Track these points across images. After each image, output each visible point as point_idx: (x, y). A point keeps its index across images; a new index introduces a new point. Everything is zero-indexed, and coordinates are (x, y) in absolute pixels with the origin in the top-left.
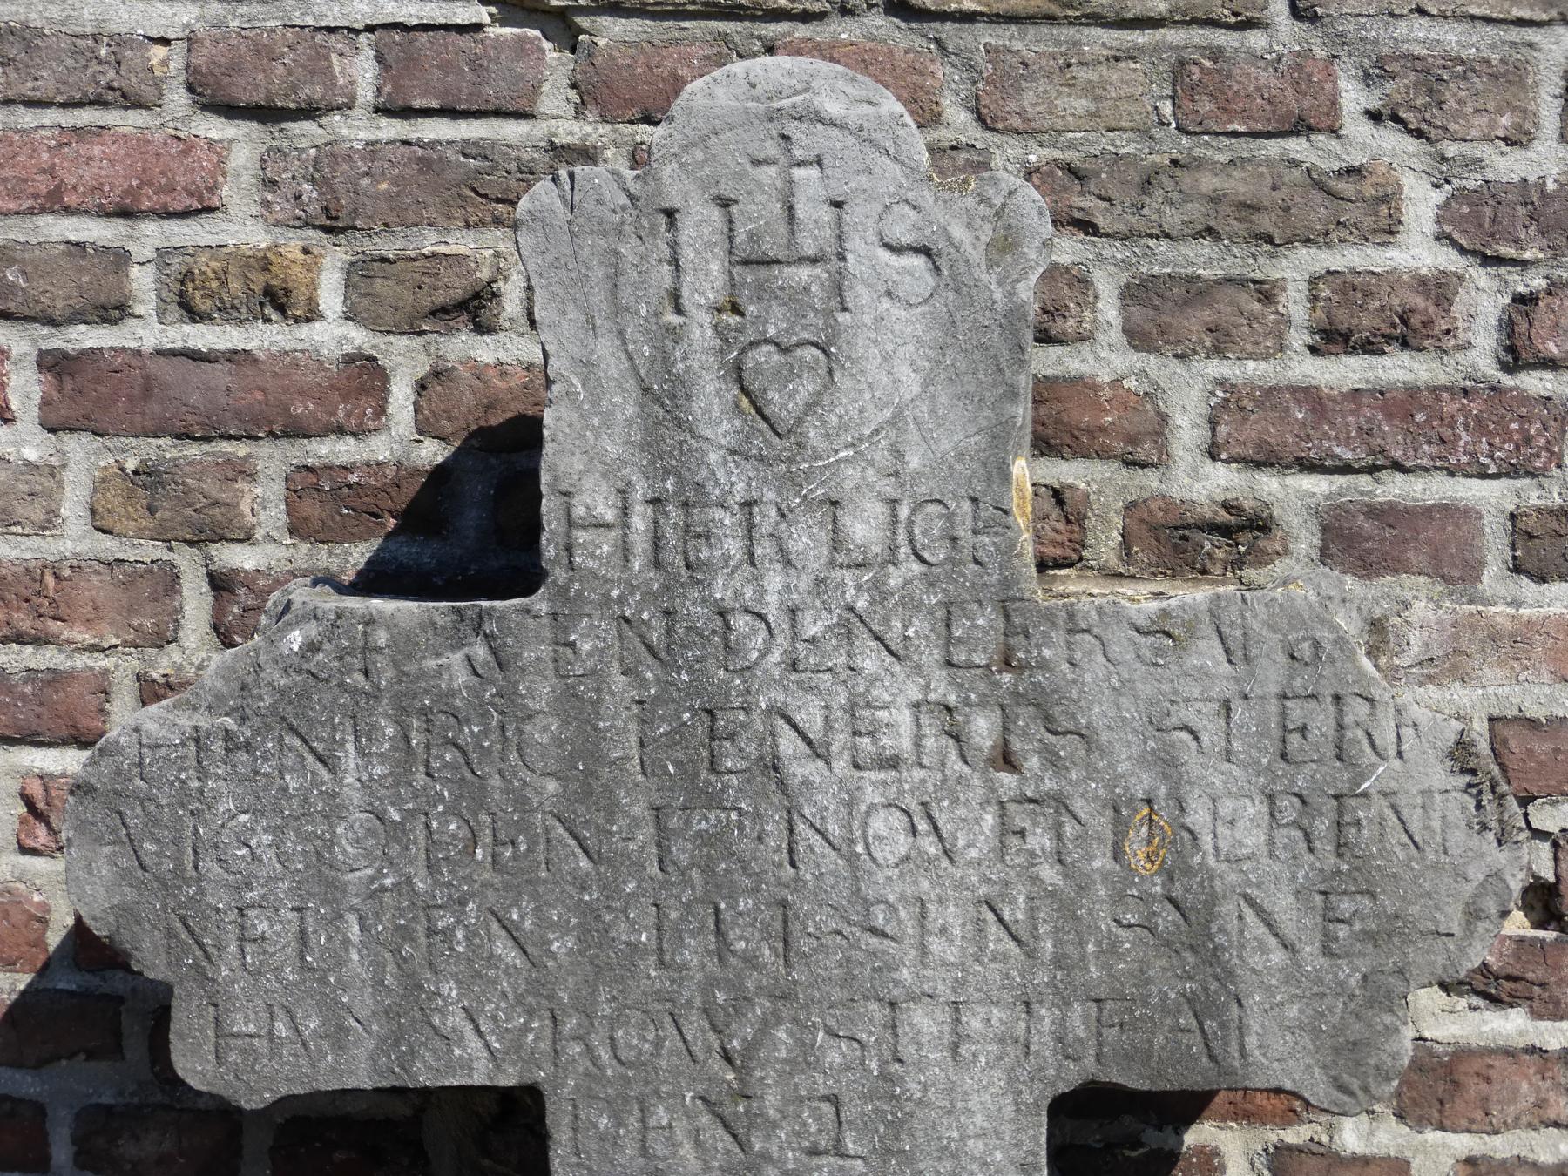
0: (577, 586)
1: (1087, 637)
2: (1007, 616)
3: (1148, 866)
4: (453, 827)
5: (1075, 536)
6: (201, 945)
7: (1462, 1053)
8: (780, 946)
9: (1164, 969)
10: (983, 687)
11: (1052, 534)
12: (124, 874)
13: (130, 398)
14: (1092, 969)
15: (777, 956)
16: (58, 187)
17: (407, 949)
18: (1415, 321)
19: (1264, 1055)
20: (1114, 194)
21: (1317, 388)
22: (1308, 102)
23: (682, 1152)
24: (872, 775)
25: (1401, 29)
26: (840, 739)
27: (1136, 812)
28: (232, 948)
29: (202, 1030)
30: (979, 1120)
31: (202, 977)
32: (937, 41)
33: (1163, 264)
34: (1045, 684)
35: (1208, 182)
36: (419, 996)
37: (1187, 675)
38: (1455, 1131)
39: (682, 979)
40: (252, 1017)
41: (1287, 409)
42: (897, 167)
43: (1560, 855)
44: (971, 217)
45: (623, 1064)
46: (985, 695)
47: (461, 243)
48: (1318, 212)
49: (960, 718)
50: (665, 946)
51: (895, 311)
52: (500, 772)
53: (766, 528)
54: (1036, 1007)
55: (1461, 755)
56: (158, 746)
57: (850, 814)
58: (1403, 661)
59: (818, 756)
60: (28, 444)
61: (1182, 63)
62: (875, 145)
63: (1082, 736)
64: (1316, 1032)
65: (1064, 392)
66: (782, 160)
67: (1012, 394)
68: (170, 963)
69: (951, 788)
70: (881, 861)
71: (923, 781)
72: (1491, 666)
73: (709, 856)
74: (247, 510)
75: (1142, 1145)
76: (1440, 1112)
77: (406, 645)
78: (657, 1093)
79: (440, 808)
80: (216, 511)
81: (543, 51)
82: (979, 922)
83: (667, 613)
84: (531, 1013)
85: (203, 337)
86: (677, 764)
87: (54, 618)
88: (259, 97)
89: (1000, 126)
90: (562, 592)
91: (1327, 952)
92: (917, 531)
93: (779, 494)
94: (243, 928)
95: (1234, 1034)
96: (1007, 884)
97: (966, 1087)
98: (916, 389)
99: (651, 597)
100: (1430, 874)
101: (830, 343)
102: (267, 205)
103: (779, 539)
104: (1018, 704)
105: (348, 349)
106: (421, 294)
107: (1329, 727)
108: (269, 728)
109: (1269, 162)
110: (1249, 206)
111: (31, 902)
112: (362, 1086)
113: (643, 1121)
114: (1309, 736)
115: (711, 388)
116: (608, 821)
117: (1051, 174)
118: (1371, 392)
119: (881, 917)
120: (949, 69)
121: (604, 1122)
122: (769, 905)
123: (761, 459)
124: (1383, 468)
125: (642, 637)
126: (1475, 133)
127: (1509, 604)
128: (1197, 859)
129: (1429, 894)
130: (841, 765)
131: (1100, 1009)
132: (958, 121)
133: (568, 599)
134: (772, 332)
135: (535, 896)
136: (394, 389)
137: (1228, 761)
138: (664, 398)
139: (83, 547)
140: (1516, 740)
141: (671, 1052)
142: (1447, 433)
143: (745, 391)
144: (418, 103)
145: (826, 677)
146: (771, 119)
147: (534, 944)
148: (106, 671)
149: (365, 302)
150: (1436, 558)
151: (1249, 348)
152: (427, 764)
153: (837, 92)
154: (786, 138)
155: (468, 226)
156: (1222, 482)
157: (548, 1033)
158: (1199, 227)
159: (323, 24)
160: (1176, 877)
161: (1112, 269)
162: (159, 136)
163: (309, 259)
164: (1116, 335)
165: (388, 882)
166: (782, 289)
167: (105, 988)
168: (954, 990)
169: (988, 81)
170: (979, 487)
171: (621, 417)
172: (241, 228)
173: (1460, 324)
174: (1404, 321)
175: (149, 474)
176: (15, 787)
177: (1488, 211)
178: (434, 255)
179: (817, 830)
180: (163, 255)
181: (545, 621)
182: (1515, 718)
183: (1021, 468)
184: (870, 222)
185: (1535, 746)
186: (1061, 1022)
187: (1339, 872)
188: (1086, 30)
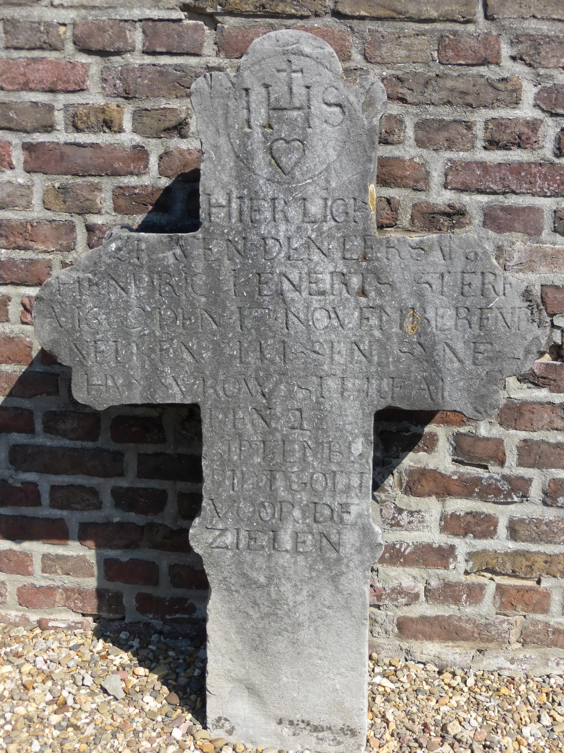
0: (212, 228)
1: (393, 249)
2: (365, 242)
5: (394, 216)
6: (82, 354)
7: (524, 403)
8: (282, 357)
10: (356, 267)
11: (386, 215)
12: (54, 329)
13: (56, 161)
16: (27, 81)
17: (153, 356)
18: (524, 137)
20: (414, 88)
21: (486, 162)
22: (488, 52)
25: (526, 24)
26: (305, 285)
27: (408, 312)
28: (92, 355)
29: (83, 383)
30: (350, 418)
31: (82, 364)
32: (351, 27)
33: (431, 115)
34: (378, 266)
35: (449, 83)
37: (428, 264)
41: (474, 170)
42: (330, 73)
44: (357, 93)
47: (175, 104)
48: (490, 95)
51: (328, 128)
52: (185, 294)
53: (280, 208)
55: (527, 295)
56: (65, 284)
58: (511, 264)
60: (21, 178)
61: (442, 37)
62: (322, 64)
64: (469, 391)
65: (392, 163)
66: (288, 70)
67: (370, 160)
68: (71, 360)
69: (343, 302)
71: (334, 300)
72: (543, 266)
73: (258, 325)
74: (99, 202)
77: (152, 250)
78: (239, 406)
80: (87, 202)
81: (204, 30)
82: (352, 350)
83: (244, 238)
84: (196, 378)
85: (82, 138)
86: (246, 292)
87: (31, 241)
88: (100, 47)
89: (373, 61)
90: (207, 230)
91: (474, 364)
92: (334, 210)
93: (285, 196)
94: (96, 348)
95: (440, 391)
96: (362, 336)
98: (335, 158)
99: (238, 233)
100: (513, 337)
101: (304, 140)
102: (103, 88)
103: (284, 212)
105: (134, 143)
106: (160, 123)
107: (479, 284)
108: (104, 278)
109: (473, 76)
110: (464, 93)
111: (26, 341)
113: (234, 416)
115: (261, 156)
117: (391, 80)
118: (505, 164)
120: (355, 38)
121: (221, 416)
122: (279, 342)
123: (278, 182)
124: (508, 193)
125: (235, 247)
126: (551, 65)
127: (551, 244)
128: (429, 329)
130: (305, 294)
132: (357, 59)
133: (209, 233)
134: (283, 135)
135: (197, 338)
136: (151, 159)
138: (244, 159)
139: (41, 215)
140: (550, 294)
141: (244, 392)
142: (533, 180)
143: (273, 157)
144: (158, 50)
145: (300, 262)
146: (284, 54)
149: (140, 126)
150: (525, 226)
151: (461, 147)
152: (160, 291)
153: (309, 44)
154: (290, 61)
155: (177, 97)
156: (448, 197)
157: (202, 385)
158: (445, 101)
159: (123, 18)
161: (412, 116)
162: (63, 62)
163: (119, 109)
164: (412, 142)
165: (146, 332)
166: (287, 119)
168: (342, 373)
169: (369, 43)
170: (356, 194)
171: (228, 167)
172: (94, 97)
173: (540, 139)
174: (520, 138)
175: (64, 189)
176: (19, 301)
177: (554, 96)
178: (165, 108)
180: (66, 107)
181: (201, 241)
182: (551, 285)
183: (372, 187)
184: (320, 94)
185: (557, 295)
186: (379, 386)
188: (407, 23)
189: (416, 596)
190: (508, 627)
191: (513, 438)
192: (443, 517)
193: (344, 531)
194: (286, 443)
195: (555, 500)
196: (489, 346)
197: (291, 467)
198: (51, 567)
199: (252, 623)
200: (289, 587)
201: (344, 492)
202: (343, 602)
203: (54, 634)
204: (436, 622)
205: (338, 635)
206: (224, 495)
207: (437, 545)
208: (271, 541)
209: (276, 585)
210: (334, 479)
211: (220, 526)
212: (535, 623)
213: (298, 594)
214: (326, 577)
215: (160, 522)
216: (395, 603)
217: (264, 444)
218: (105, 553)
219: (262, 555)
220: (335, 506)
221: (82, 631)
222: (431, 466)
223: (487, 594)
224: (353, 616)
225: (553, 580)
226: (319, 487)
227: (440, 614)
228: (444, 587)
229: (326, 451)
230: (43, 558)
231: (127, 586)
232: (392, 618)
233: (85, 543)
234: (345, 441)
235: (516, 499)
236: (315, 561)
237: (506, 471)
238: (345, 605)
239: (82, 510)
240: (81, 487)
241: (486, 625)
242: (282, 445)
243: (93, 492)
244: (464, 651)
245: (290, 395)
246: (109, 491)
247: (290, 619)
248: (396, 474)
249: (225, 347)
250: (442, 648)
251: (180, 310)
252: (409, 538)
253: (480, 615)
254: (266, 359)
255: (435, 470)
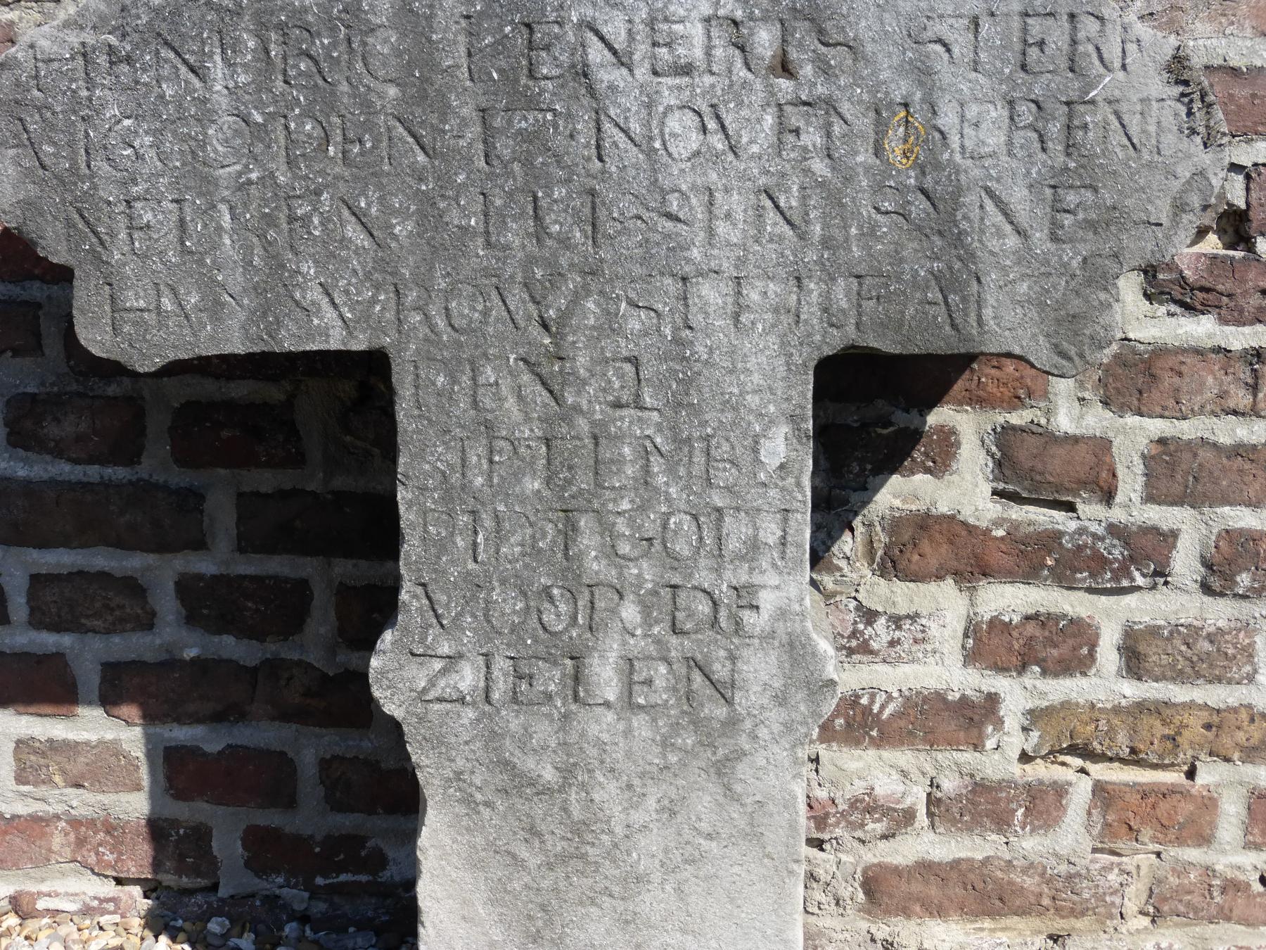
3: (904, 161)
4: (308, 127)
7: (1160, 351)
8: (589, 229)
9: (916, 250)
12: (28, 173)
14: (855, 249)
15: (587, 238)
19: (998, 325)
23: (507, 405)
24: (669, 81)
27: (895, 114)
28: (123, 235)
36: (282, 274)
38: (1150, 417)
39: (506, 257)
40: (142, 294)
43: (1252, 186)
45: (456, 330)
46: (767, 10)
49: (746, 31)
50: (491, 229)
52: (348, 79)
54: (805, 282)
56: (51, 60)
57: (649, 114)
59: (622, 64)
63: (850, 47)
64: (1042, 306)
68: (70, 250)
69: (736, 92)
70: (676, 156)
71: (713, 86)
73: (528, 151)
75: (891, 424)
76: (1139, 400)
78: (485, 355)
79: (297, 111)
82: (759, 207)
84: (377, 287)
86: (500, 71)
91: (1054, 238)
94: (131, 218)
95: (973, 307)
97: (745, 350)
100: (1145, 172)
104: (795, 18)
107: (1064, 43)
108: (146, 43)
112: (236, 351)
113: (474, 379)
114: (1046, 50)
116: (441, 121)
119: (675, 203)
121: (441, 380)
122: (580, 194)
128: (946, 156)
129: (1143, 189)
130: (642, 72)
131: (860, 284)
135: (380, 186)
137: (976, 70)
147: (380, 228)
148: (11, 24)
160: (927, 171)
165: (254, 176)
167: (25, 296)
168: (736, 267)
179: (621, 128)
182: (1220, 67)
186: (827, 295)
187: (1067, 169)
189: (909, 816)
190: (1120, 879)
191: (1132, 436)
192: (972, 629)
193: (745, 653)
194: (603, 441)
195: (1229, 579)
196: (1089, 194)
197: (615, 500)
198: (37, 768)
199: (527, 879)
200: (614, 792)
201: (742, 558)
202: (742, 823)
203: (50, 927)
204: (954, 875)
205: (732, 900)
206: (454, 573)
207: (958, 696)
208: (569, 682)
209: (583, 786)
210: (719, 528)
211: (445, 649)
212: (1182, 869)
213: (636, 806)
214: (704, 765)
215: (295, 656)
216: (859, 834)
217: (548, 447)
218: (167, 734)
219: (547, 716)
220: (723, 591)
221: (117, 918)
222: (943, 508)
223: (1072, 806)
224: (769, 856)
225: (1223, 767)
226: (681, 547)
227: (963, 855)
228: (973, 791)
229: (699, 459)
230: (17, 747)
231: (221, 810)
232: (850, 869)
233: (116, 711)
234: (745, 435)
235: (1140, 581)
236: (675, 727)
237: (1117, 514)
238: (748, 829)
239: (108, 632)
240: (103, 577)
241: (1070, 877)
242: (591, 446)
243: (133, 588)
244: (1019, 940)
245: (610, 325)
246: (171, 585)
247: (618, 867)
248: (860, 529)
249: (447, 209)
250: (967, 934)
251: (336, 120)
252: (890, 680)
253: (1056, 855)
254: (550, 235)
255: (953, 517)
